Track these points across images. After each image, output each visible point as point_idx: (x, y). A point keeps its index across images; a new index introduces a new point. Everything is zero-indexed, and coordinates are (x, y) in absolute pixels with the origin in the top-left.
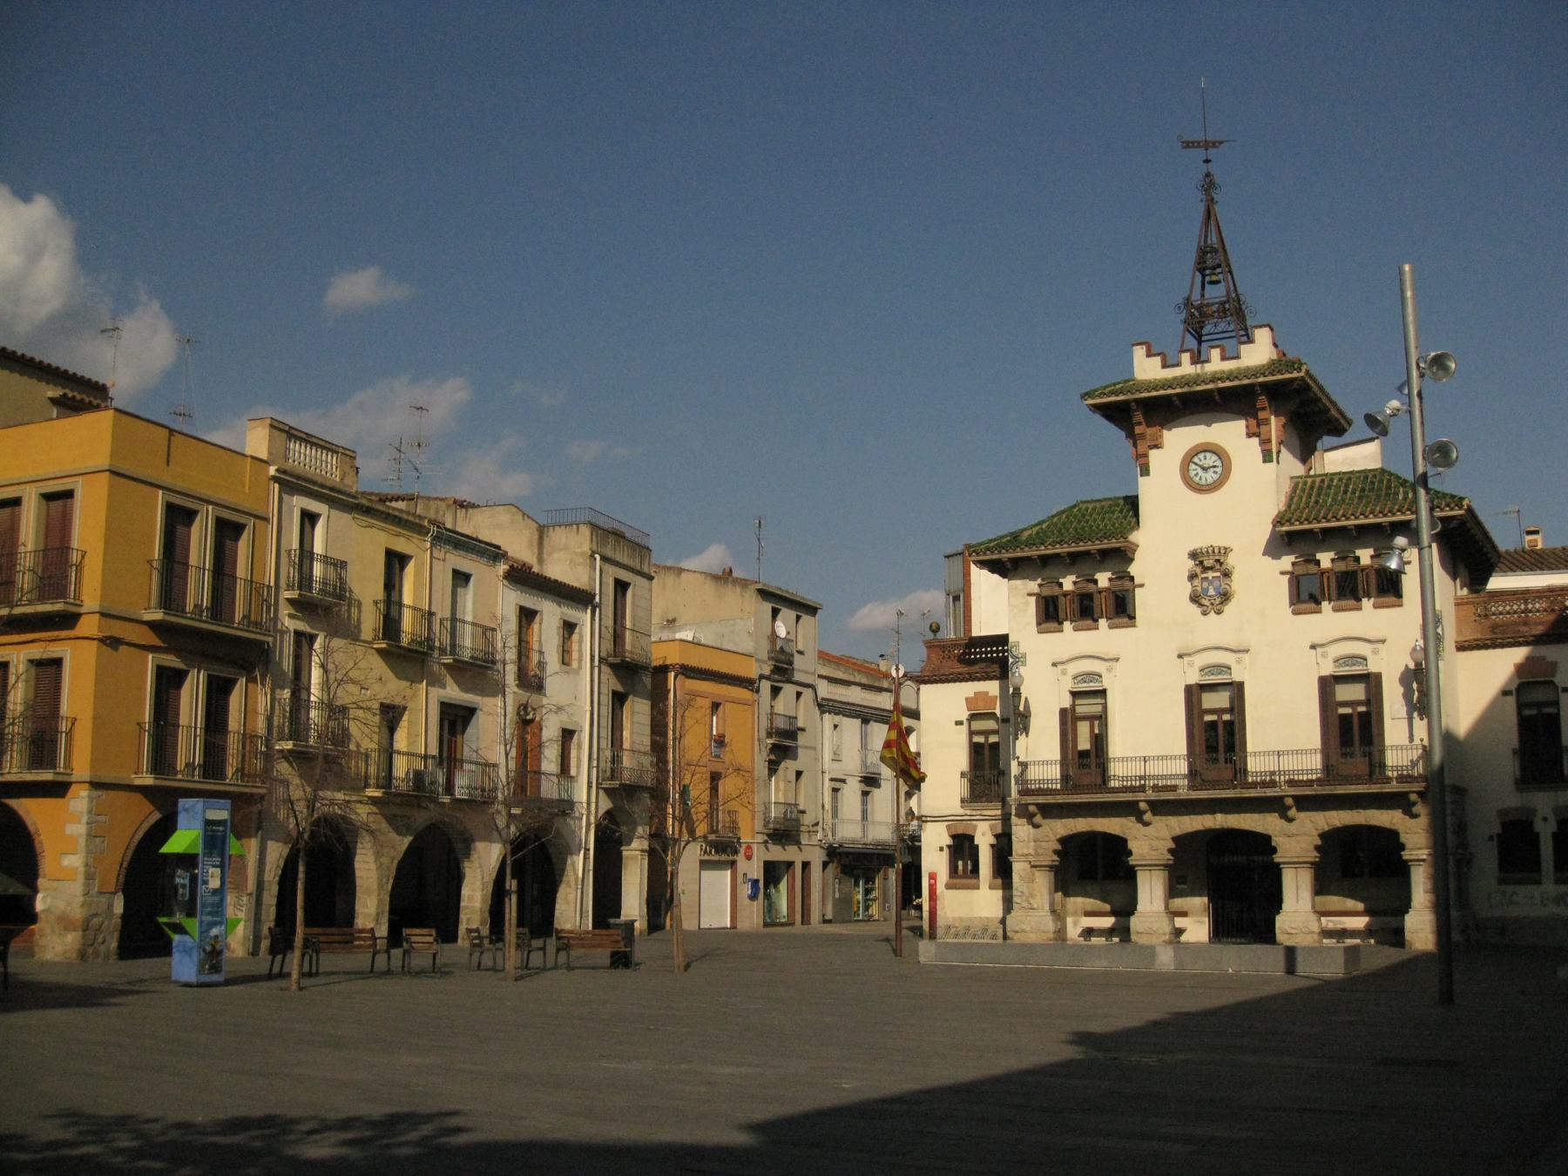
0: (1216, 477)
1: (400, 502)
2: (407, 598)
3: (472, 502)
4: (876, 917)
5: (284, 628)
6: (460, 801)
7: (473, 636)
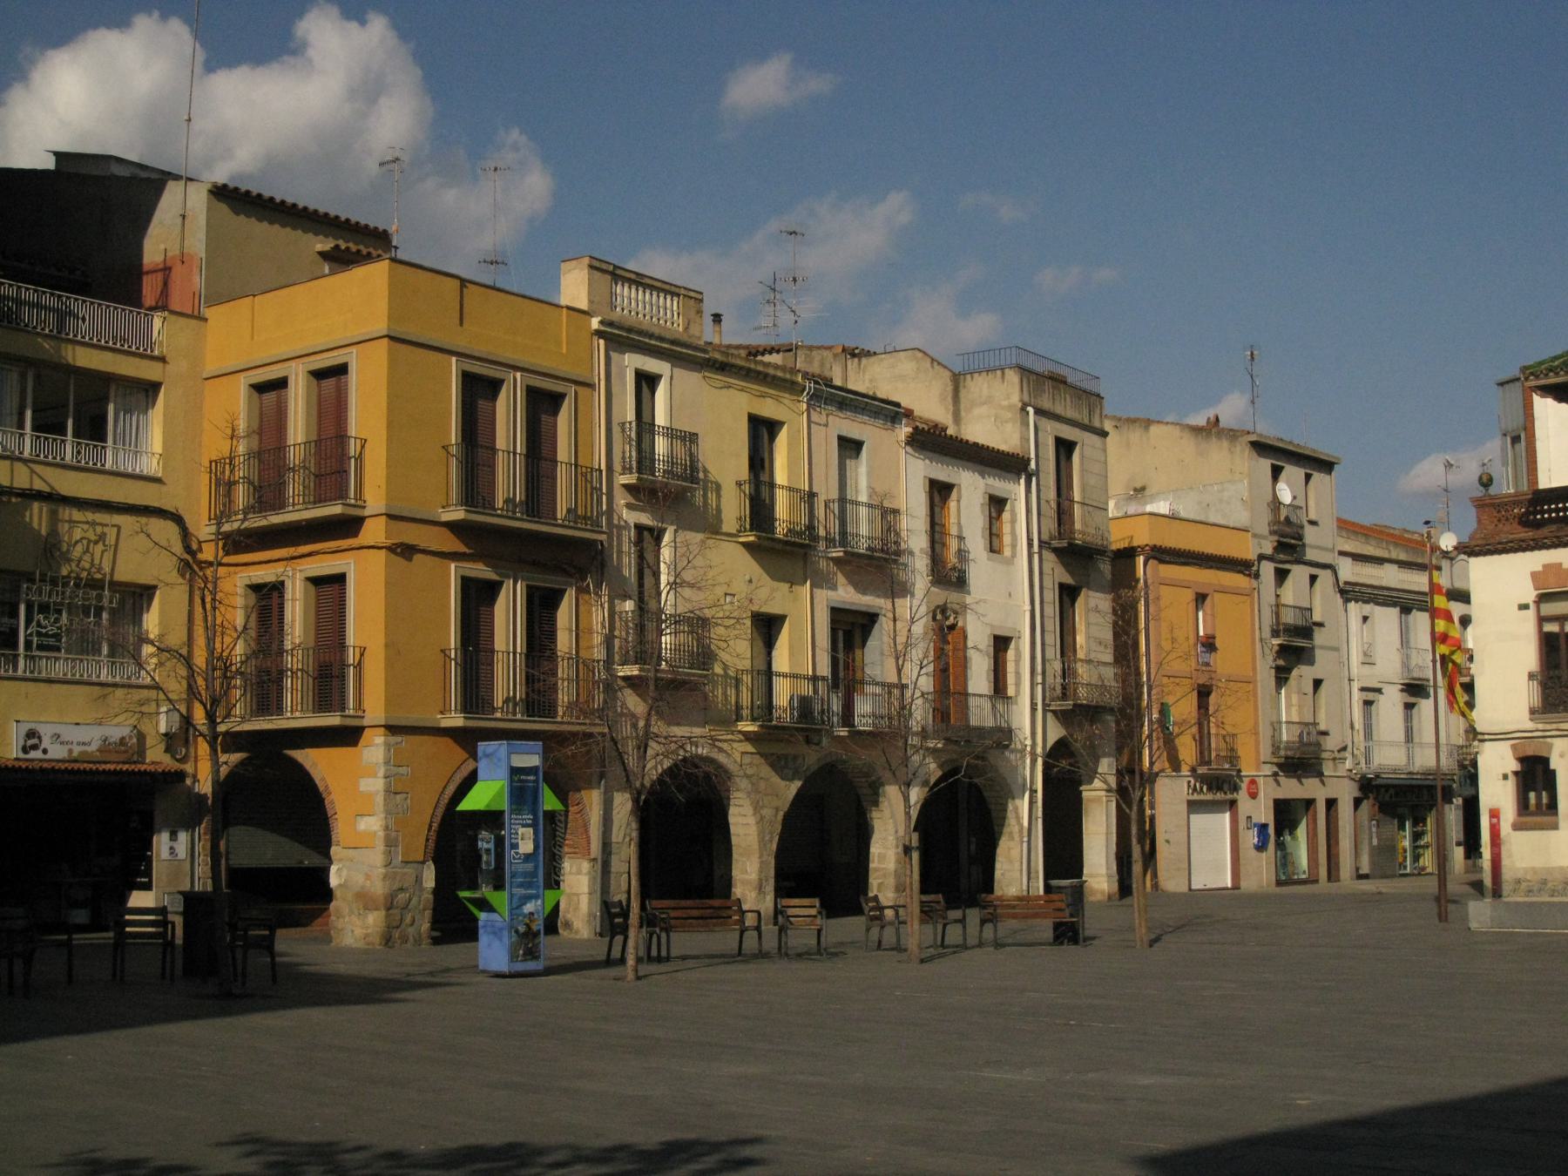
1: (774, 355)
2: (781, 477)
3: (866, 349)
4: (1429, 870)
5: (622, 523)
6: (860, 733)
7: (871, 521)
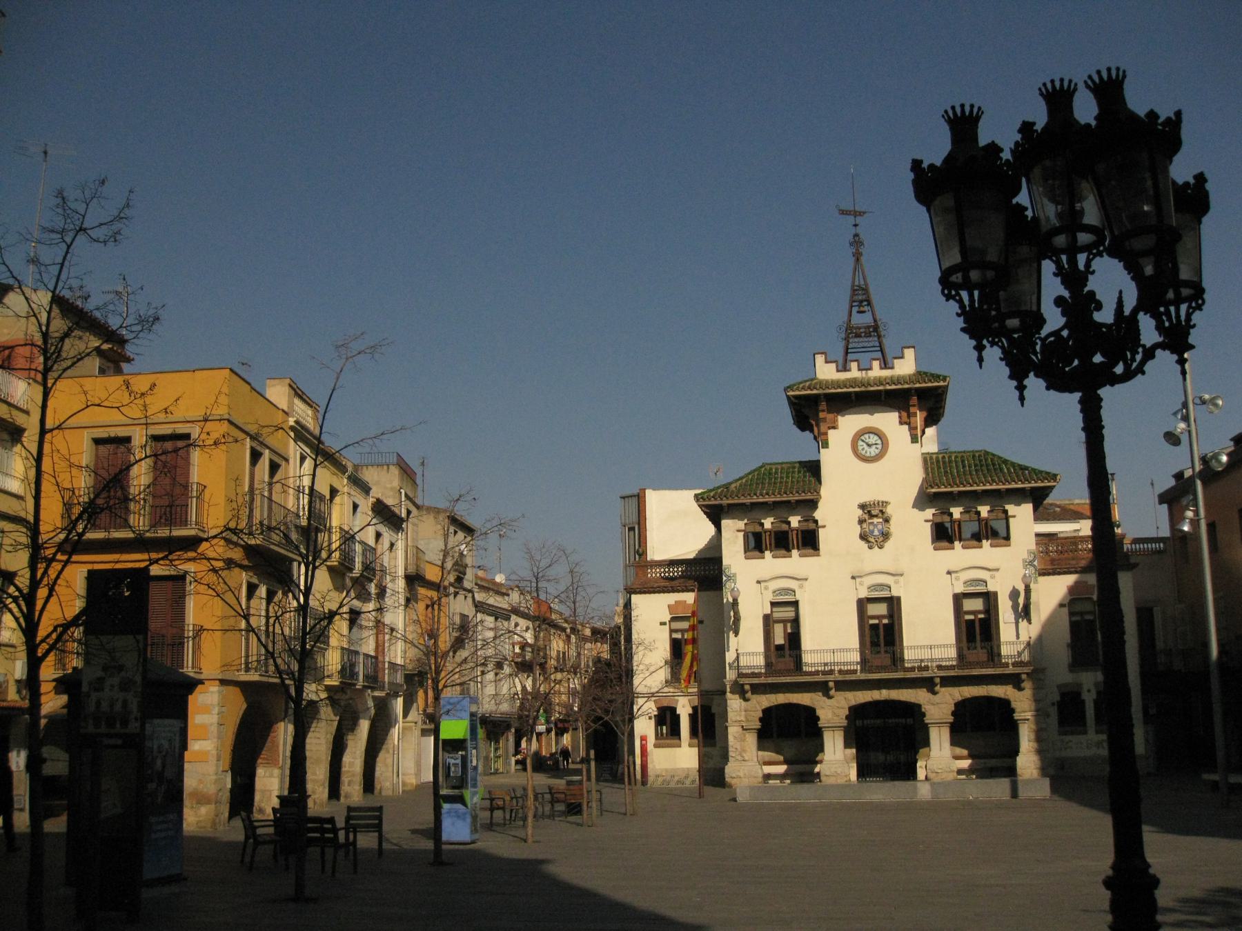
0: (877, 451)
4: (501, 770)
